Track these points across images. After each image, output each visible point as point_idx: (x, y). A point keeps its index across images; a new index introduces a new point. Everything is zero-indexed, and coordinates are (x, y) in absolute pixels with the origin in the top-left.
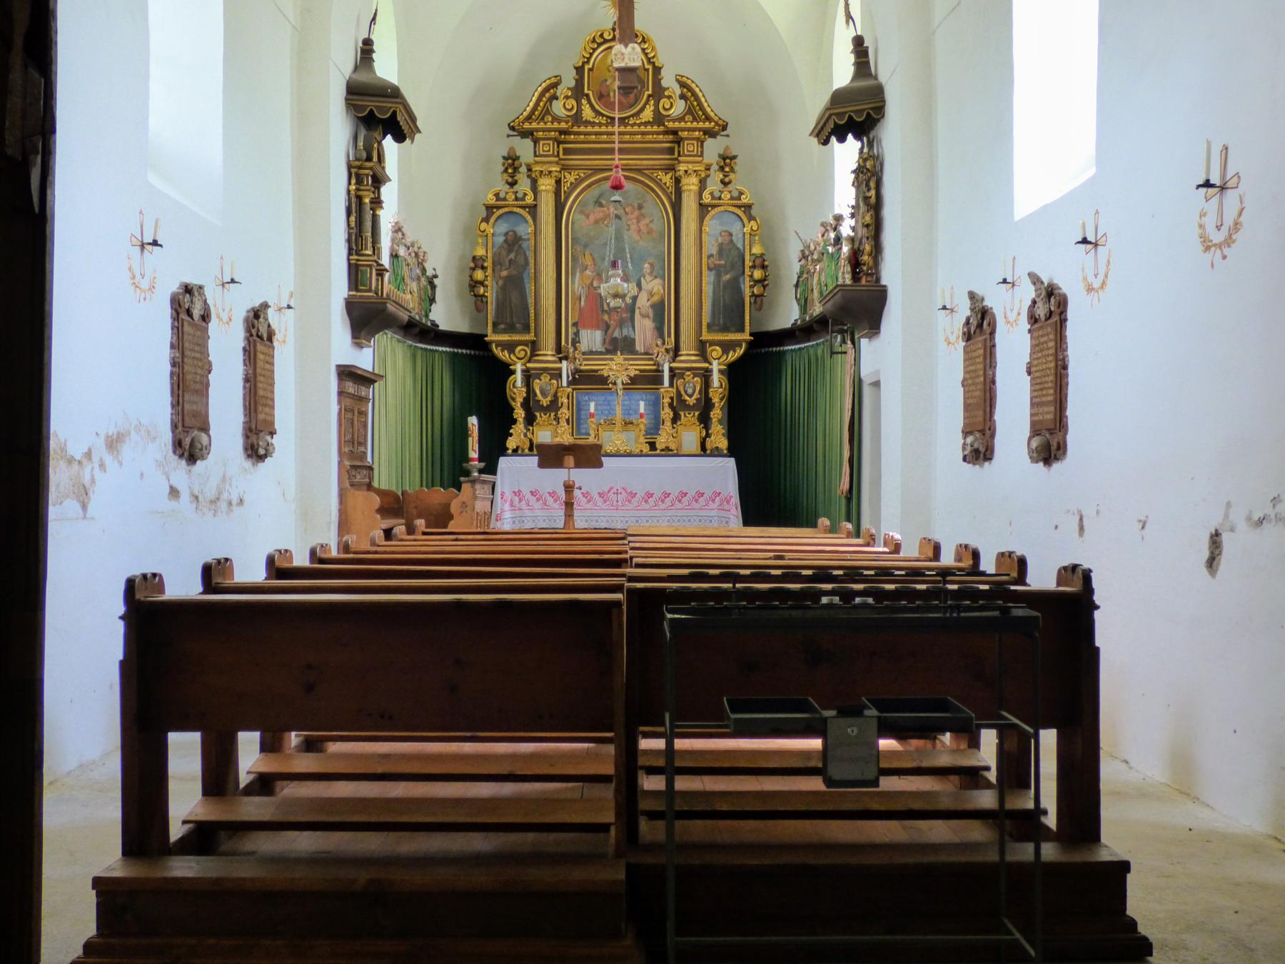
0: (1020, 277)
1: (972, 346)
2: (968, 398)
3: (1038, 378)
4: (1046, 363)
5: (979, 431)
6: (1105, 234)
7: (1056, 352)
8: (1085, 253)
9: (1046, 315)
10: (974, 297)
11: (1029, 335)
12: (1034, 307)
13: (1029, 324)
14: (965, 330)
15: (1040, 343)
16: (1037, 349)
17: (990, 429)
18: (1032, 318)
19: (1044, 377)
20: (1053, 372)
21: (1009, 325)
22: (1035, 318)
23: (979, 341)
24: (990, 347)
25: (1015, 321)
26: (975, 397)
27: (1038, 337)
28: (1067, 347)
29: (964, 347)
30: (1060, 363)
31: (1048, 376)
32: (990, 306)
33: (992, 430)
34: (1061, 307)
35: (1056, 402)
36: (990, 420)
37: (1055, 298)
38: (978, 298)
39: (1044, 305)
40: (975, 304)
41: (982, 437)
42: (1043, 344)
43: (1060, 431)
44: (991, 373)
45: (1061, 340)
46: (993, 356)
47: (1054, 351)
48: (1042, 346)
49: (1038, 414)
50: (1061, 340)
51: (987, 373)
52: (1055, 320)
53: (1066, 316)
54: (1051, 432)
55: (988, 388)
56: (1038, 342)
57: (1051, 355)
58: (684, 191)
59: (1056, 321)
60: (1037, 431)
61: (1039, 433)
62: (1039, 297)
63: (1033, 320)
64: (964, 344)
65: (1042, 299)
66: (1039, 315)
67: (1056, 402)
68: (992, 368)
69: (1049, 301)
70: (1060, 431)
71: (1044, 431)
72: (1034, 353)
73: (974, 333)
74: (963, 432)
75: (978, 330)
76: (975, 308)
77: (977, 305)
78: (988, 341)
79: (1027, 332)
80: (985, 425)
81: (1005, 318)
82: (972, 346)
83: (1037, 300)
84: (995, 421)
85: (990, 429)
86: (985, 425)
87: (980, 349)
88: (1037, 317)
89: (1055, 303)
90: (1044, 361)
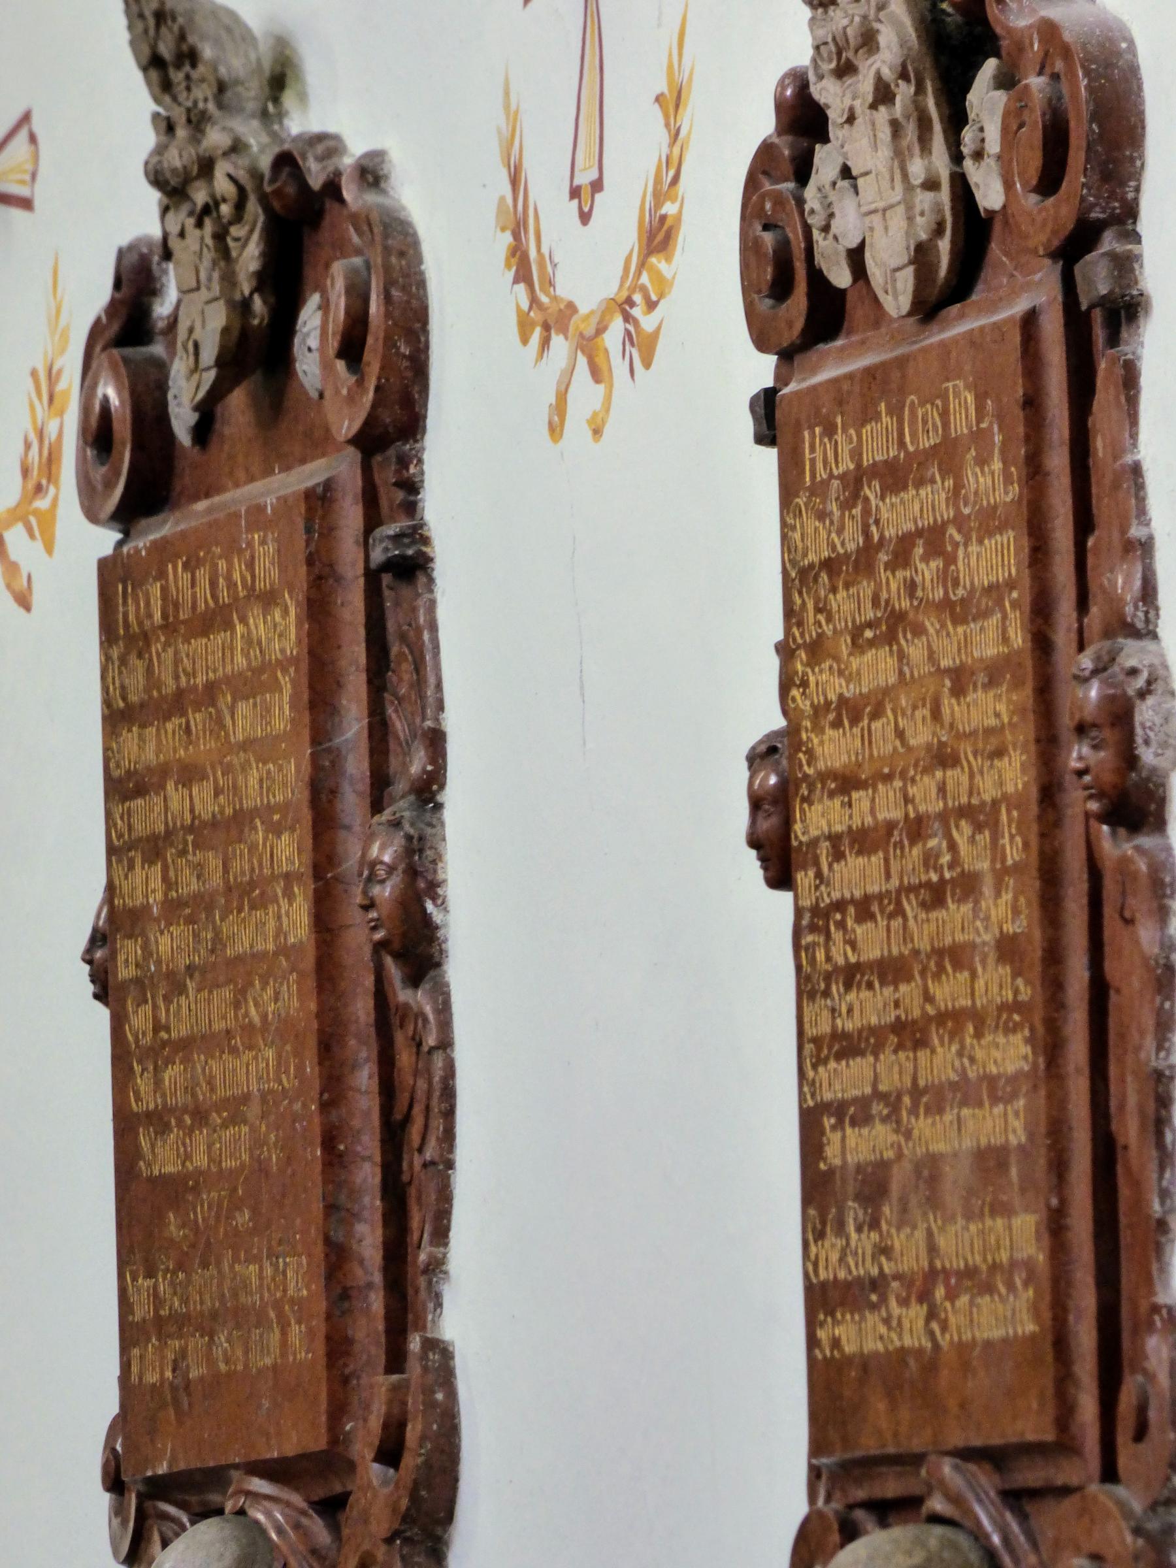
0: (26, 118)
1: (177, 575)
2: (158, 1120)
3: (864, 909)
4: (943, 758)
5: (276, 1471)
6: (26, 118)
7: (1042, 643)
8: (37, 124)
9: (922, 255)
10: (190, 57)
11: (770, 455)
12: (802, 171)
13: (761, 342)
14: (110, 391)
15: (869, 550)
16: (841, 602)
17: (390, 1454)
18: (781, 288)
19: (935, 896)
20: (1013, 853)
21: (560, 344)
22: (817, 280)
23: (257, 516)
24: (372, 577)
25: (624, 307)
26: (235, 1109)
27: (854, 483)
28: (1148, 593)
29: (106, 568)
30: (1077, 754)
31: (968, 885)
32: (356, 147)
33: (411, 1461)
34: (1076, 177)
35: (1059, 1166)
36: (396, 1360)
37: (1006, 81)
38: (235, 64)
39: (900, 156)
40: (198, 122)
41: (318, 1528)
42: (901, 557)
43: (1110, 1474)
44: (385, 852)
45: (1084, 523)
46: (401, 679)
47: (1018, 638)
48: (893, 583)
49: (877, 1284)
50: (1084, 523)
51: (350, 862)
52: (1020, 307)
53: (1125, 265)
54: (1030, 1475)
55: (362, 1009)
56: (851, 541)
57: (994, 673)
58: (826, 767)
59: (1030, 320)
60: (867, 1466)
61: (891, 1487)
62: (845, 70)
63: (799, 301)
64: (106, 540)
65: (883, 95)
66: (856, 257)
67: (1059, 1166)
68: (402, 806)
69: (956, 119)
70: (1110, 1474)
71: (947, 1468)
72: (817, 650)
73: (203, 430)
74: (114, 1482)
75: (238, 400)
76: (206, 167)
77: (216, 138)
78: (351, 516)
79: (746, 425)
80: (338, 1411)
81: (523, 275)
82: (177, 575)
83: (827, 92)
84: (442, 1352)
85: (390, 1454)
86: (338, 1411)
87: (269, 599)
88: (841, 277)
89: (1009, 134)
90: (921, 735)
